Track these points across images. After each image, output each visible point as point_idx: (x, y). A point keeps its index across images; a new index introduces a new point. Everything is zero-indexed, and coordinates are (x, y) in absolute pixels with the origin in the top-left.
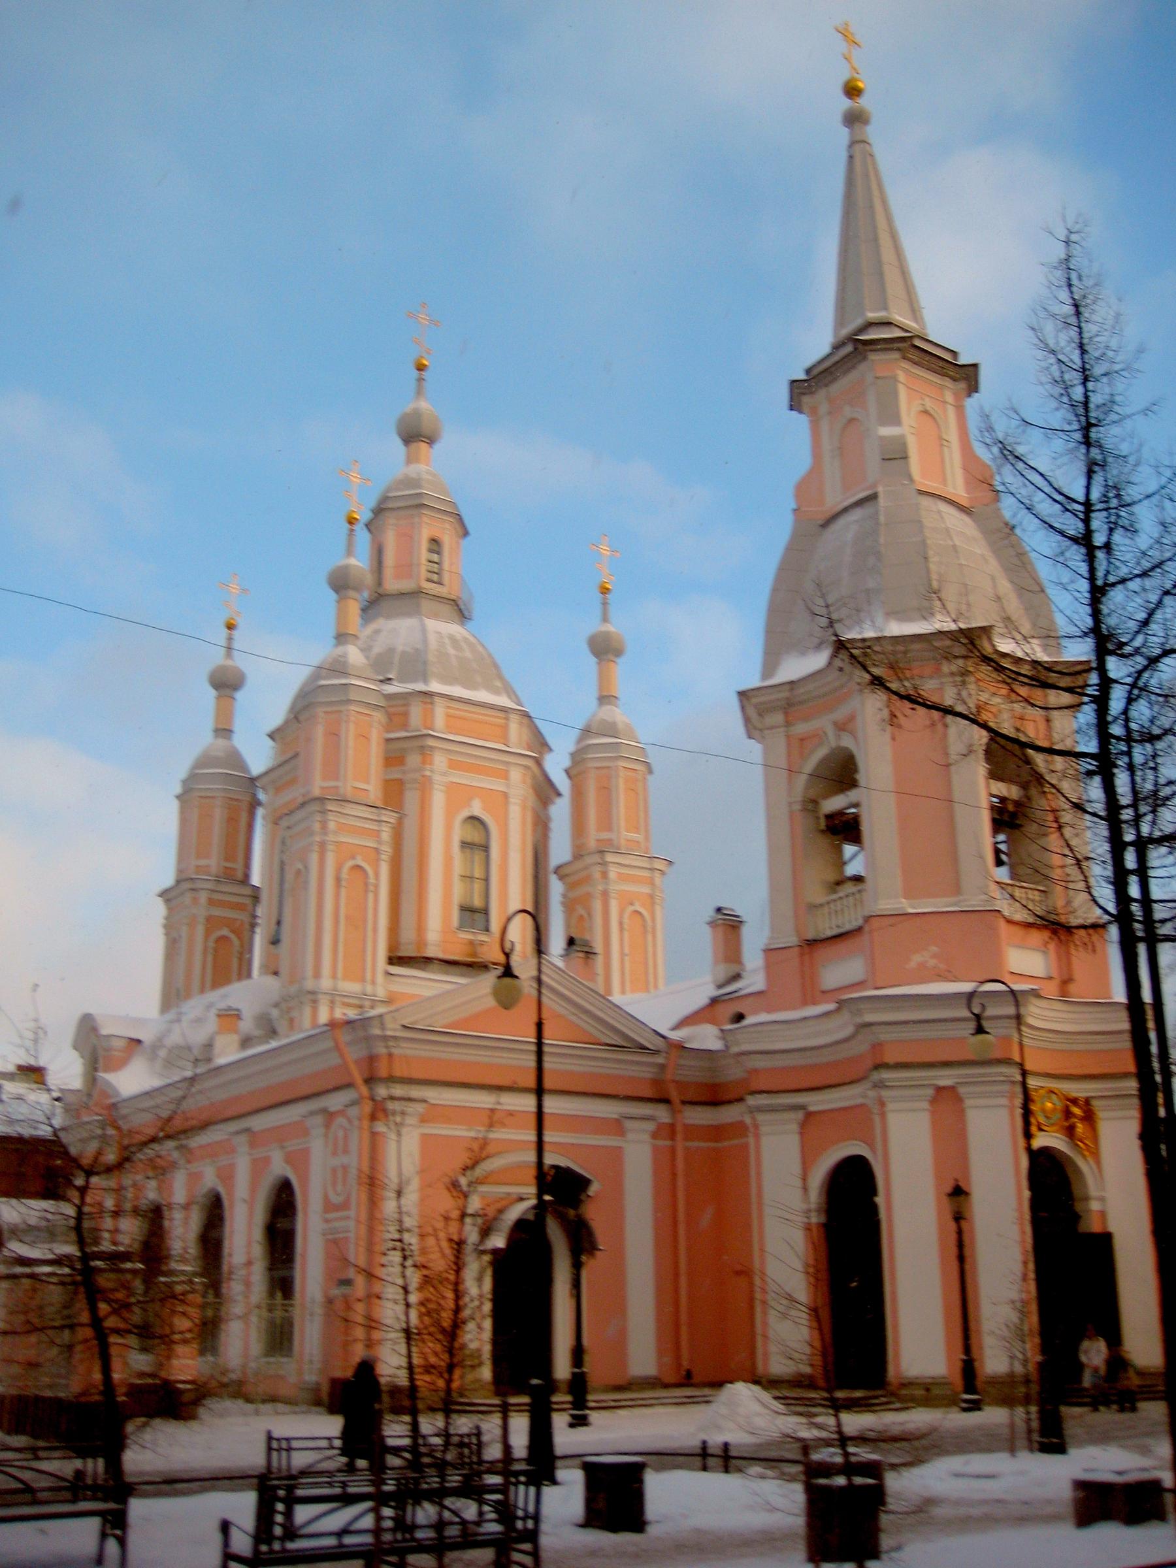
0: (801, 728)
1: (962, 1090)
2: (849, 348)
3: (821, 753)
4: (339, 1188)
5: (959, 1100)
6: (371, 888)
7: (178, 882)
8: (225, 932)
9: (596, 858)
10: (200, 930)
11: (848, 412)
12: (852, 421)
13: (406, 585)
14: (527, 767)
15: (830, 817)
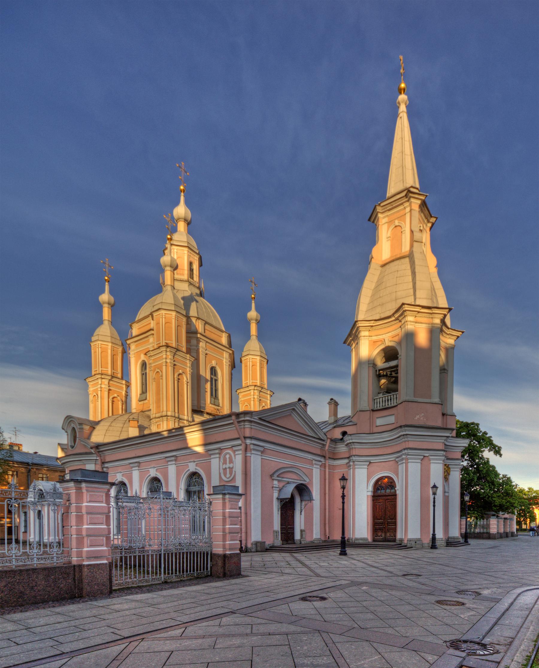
2: (403, 194)
3: (383, 347)
4: (228, 476)
9: (253, 388)
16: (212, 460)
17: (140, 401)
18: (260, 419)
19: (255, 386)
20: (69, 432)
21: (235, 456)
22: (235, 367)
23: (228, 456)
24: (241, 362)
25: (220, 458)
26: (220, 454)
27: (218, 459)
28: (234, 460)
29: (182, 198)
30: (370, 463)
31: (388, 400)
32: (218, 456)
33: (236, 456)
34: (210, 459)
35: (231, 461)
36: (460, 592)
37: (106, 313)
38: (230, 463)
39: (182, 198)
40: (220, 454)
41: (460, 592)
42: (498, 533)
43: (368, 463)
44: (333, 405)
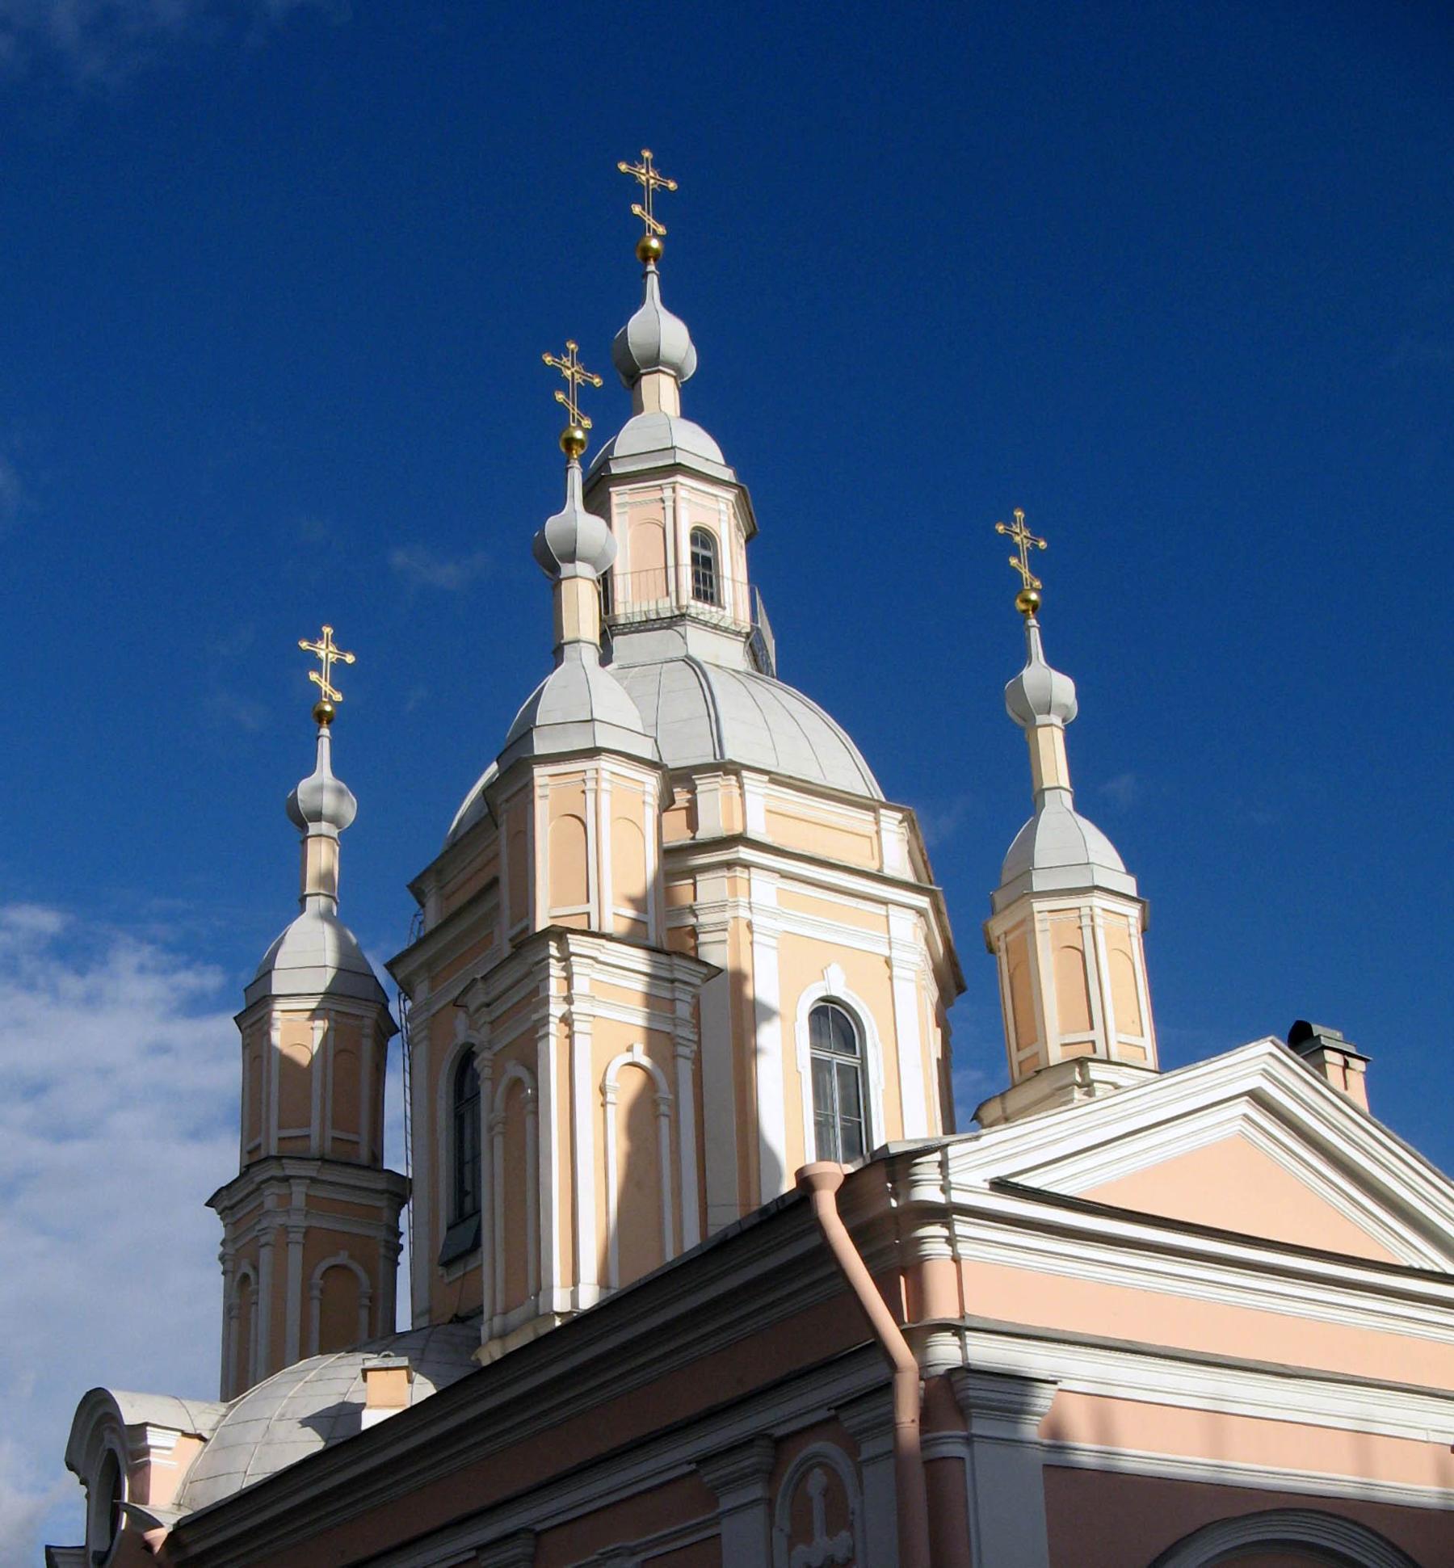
6: (664, 1108)
7: (246, 1170)
8: (342, 1258)
10: (295, 1255)
13: (666, 607)
14: (921, 912)
16: (726, 1528)
17: (447, 1264)
18: (1001, 1186)
19: (1082, 1062)
20: (95, 1478)
21: (859, 1468)
22: (961, 988)
23: (817, 1481)
24: (991, 951)
25: (770, 1503)
26: (771, 1476)
27: (759, 1512)
28: (853, 1502)
29: (653, 284)
32: (757, 1491)
33: (867, 1471)
34: (716, 1521)
35: (839, 1517)
36: (668, 594)
37: (322, 856)
38: (831, 1530)
39: (653, 284)
40: (771, 1476)
41: (668, 594)
42: (149, 1447)
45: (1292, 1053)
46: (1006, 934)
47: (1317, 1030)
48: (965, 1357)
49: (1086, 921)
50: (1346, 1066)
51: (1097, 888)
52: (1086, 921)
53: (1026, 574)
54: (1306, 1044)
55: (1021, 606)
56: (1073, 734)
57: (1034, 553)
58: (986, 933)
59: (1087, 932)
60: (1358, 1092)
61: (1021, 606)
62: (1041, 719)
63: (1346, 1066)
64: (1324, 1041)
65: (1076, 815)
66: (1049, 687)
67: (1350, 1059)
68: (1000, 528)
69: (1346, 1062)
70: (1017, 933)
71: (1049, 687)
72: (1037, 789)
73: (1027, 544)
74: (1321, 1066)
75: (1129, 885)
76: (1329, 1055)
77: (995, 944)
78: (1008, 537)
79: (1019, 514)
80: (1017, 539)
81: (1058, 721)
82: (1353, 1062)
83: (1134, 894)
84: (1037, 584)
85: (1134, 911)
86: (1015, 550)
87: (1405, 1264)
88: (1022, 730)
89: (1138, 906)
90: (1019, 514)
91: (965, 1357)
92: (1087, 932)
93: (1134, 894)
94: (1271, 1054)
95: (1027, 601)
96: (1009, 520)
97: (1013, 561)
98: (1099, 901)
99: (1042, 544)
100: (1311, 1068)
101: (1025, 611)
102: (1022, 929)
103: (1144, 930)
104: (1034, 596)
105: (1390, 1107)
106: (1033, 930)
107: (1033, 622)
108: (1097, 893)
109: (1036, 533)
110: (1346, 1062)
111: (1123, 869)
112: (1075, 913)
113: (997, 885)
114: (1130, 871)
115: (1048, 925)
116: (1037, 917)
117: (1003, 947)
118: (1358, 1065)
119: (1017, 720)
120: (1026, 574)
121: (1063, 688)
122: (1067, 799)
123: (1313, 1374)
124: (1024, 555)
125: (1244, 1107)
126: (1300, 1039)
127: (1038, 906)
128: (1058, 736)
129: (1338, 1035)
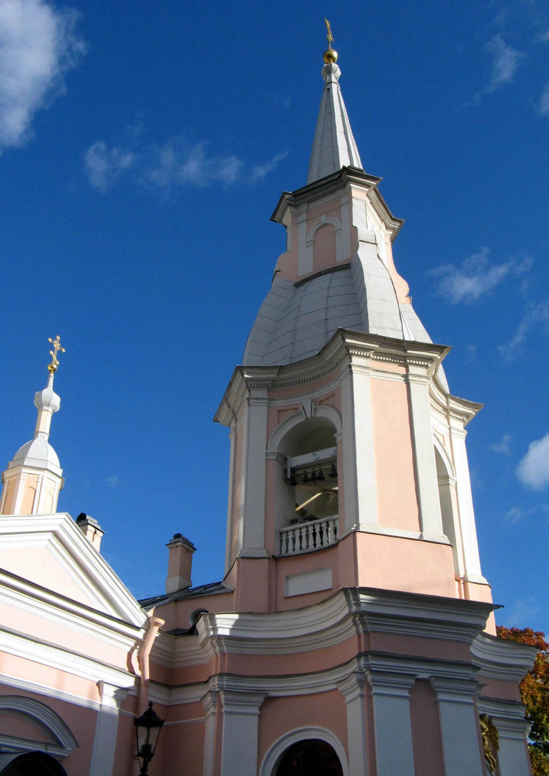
0: (280, 403)
1: (436, 684)
2: (336, 177)
5: (433, 693)
11: (323, 219)
12: (325, 225)
15: (293, 470)
24: (3, 483)
30: (269, 700)
31: (314, 535)
43: (261, 699)
44: (180, 549)
45: (76, 524)
46: (10, 477)
47: (88, 517)
48: (148, 730)
49: (40, 480)
50: (95, 533)
51: (47, 469)
52: (40, 480)
53: (55, 358)
54: (82, 522)
55: (49, 368)
56: (55, 416)
57: (60, 352)
58: (3, 476)
59: (39, 484)
60: (97, 544)
61: (49, 368)
62: (45, 408)
63: (95, 533)
64: (89, 522)
65: (48, 444)
66: (51, 399)
67: (97, 531)
68: (50, 340)
69: (96, 531)
70: (14, 478)
71: (51, 399)
72: (36, 431)
73: (58, 348)
74: (85, 531)
75: (60, 472)
76: (89, 527)
77: (5, 480)
78: (52, 344)
79: (58, 338)
80: (55, 346)
81: (51, 410)
82: (98, 532)
83: (61, 475)
84: (58, 363)
85: (59, 481)
86: (53, 349)
87: (98, 610)
88: (38, 410)
89: (61, 480)
90: (58, 338)
91: (148, 730)
92: (39, 484)
93: (61, 475)
94: (65, 519)
95: (52, 367)
96: (54, 338)
97: (51, 353)
98: (46, 474)
99: (64, 350)
100: (81, 530)
101: (51, 370)
102: (16, 477)
103: (61, 489)
104: (55, 366)
105: (107, 551)
106: (20, 478)
107: (52, 375)
108: (46, 471)
109: (62, 346)
110: (96, 531)
111: (59, 466)
112: (37, 476)
113: (11, 459)
114: (61, 467)
115: (25, 478)
116: (22, 474)
117: (7, 482)
118: (100, 534)
119: (37, 406)
120: (55, 358)
121: (56, 400)
122: (46, 437)
123: (48, 644)
124: (56, 352)
125: (50, 536)
126: (81, 520)
127: (24, 470)
128: (49, 416)
129: (96, 522)
